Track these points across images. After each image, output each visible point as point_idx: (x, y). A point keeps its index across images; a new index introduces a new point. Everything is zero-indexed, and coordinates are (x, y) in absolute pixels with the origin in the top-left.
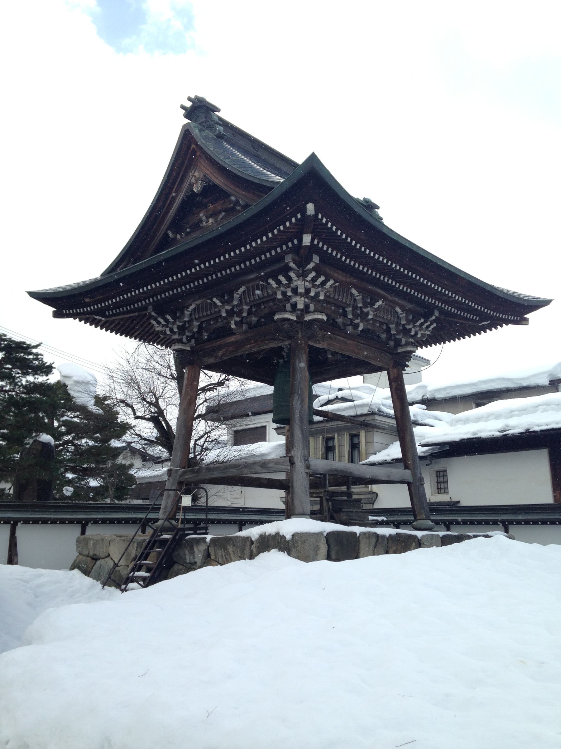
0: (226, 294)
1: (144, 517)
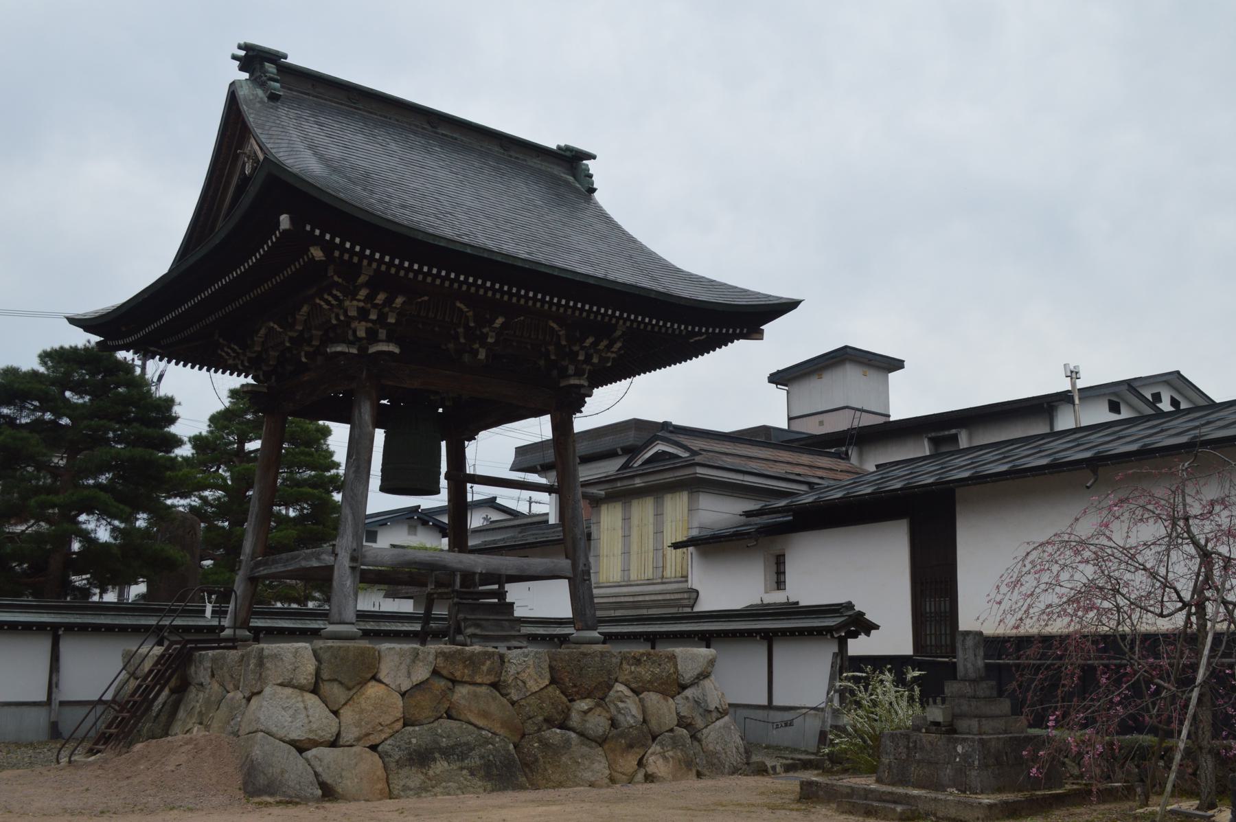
1: (154, 623)
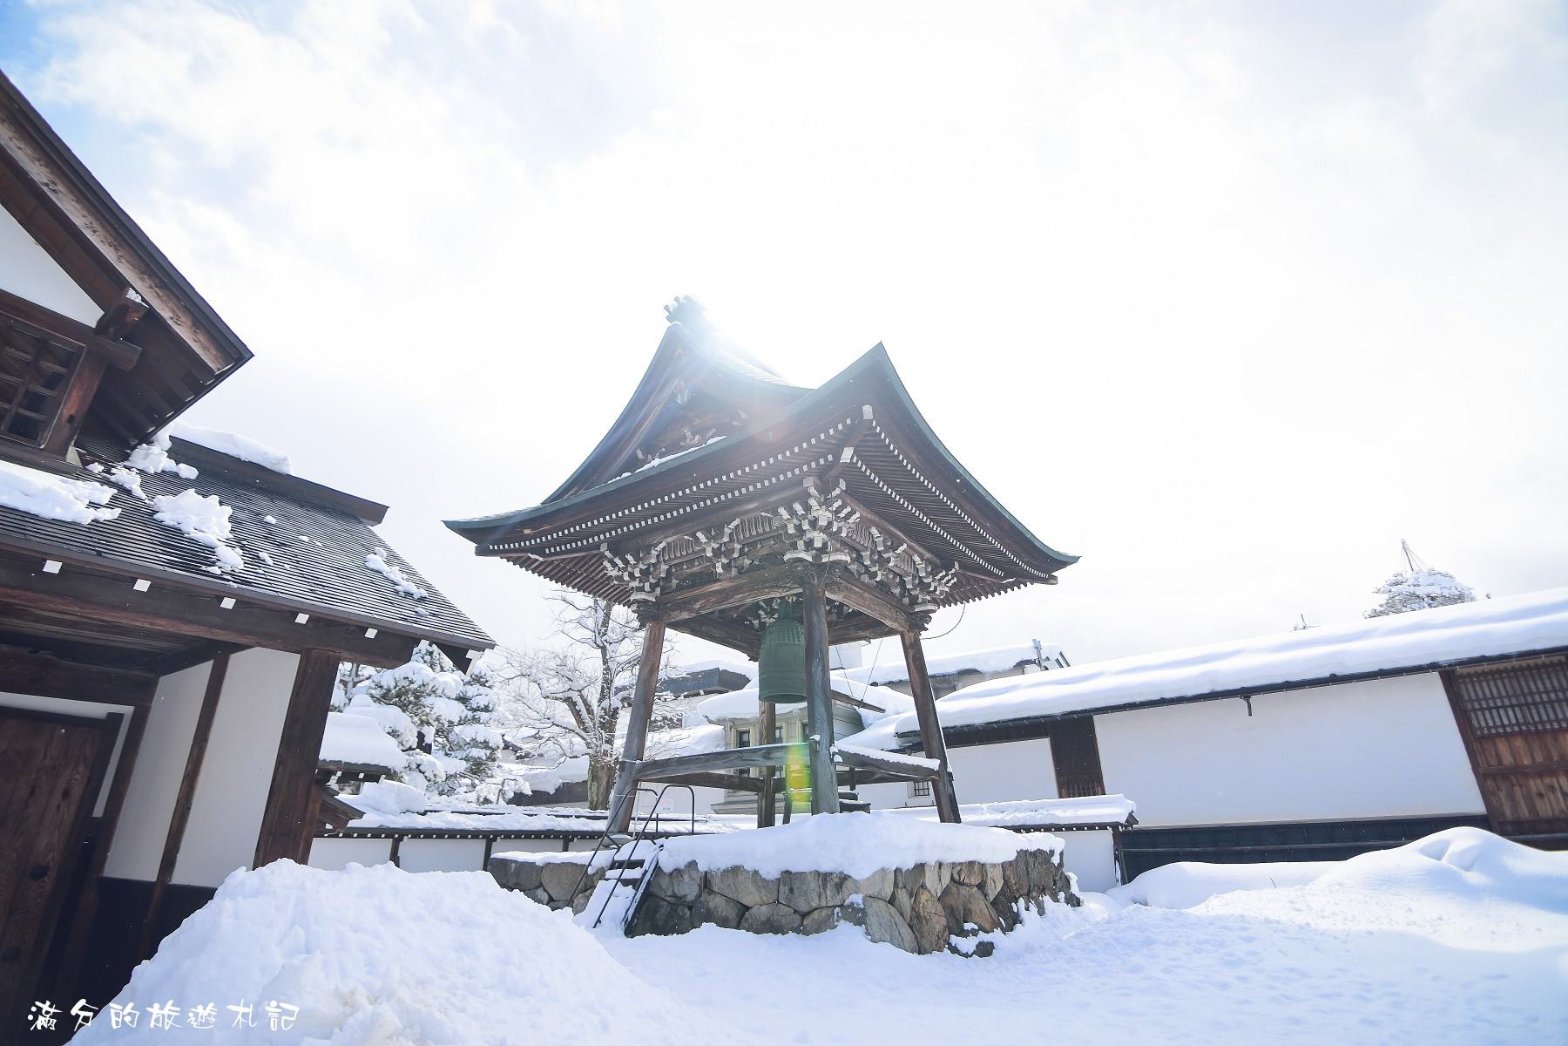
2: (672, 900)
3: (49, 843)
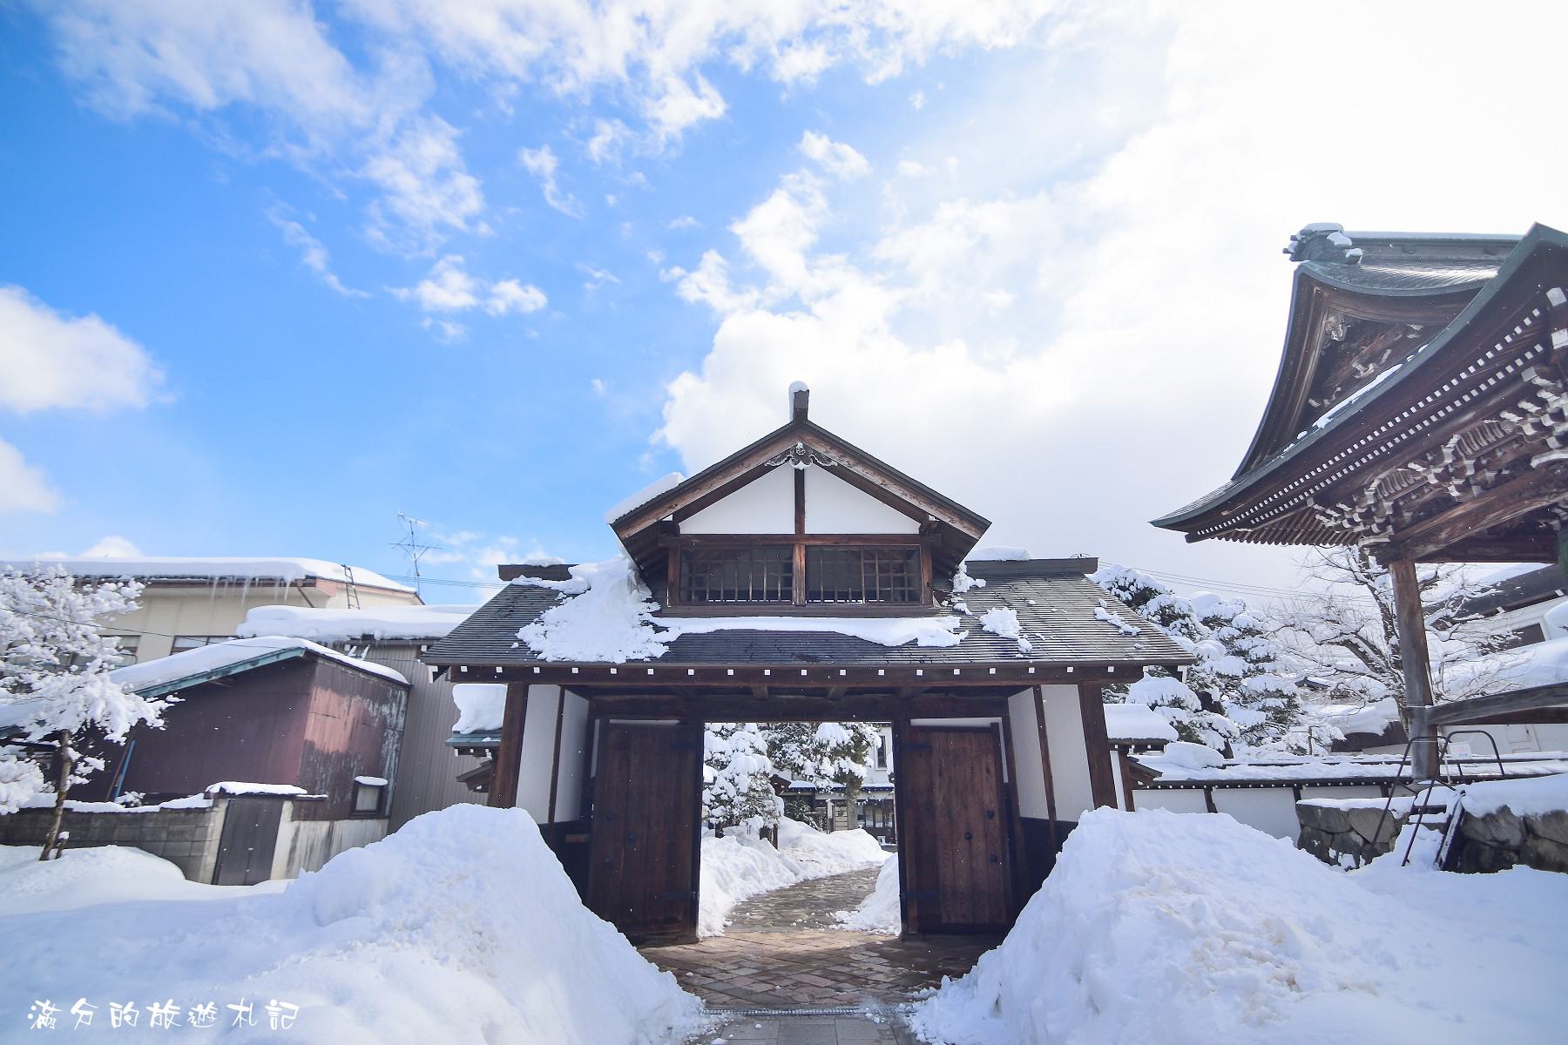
0: (1428, 451)
2: (1494, 844)
3: (990, 798)
